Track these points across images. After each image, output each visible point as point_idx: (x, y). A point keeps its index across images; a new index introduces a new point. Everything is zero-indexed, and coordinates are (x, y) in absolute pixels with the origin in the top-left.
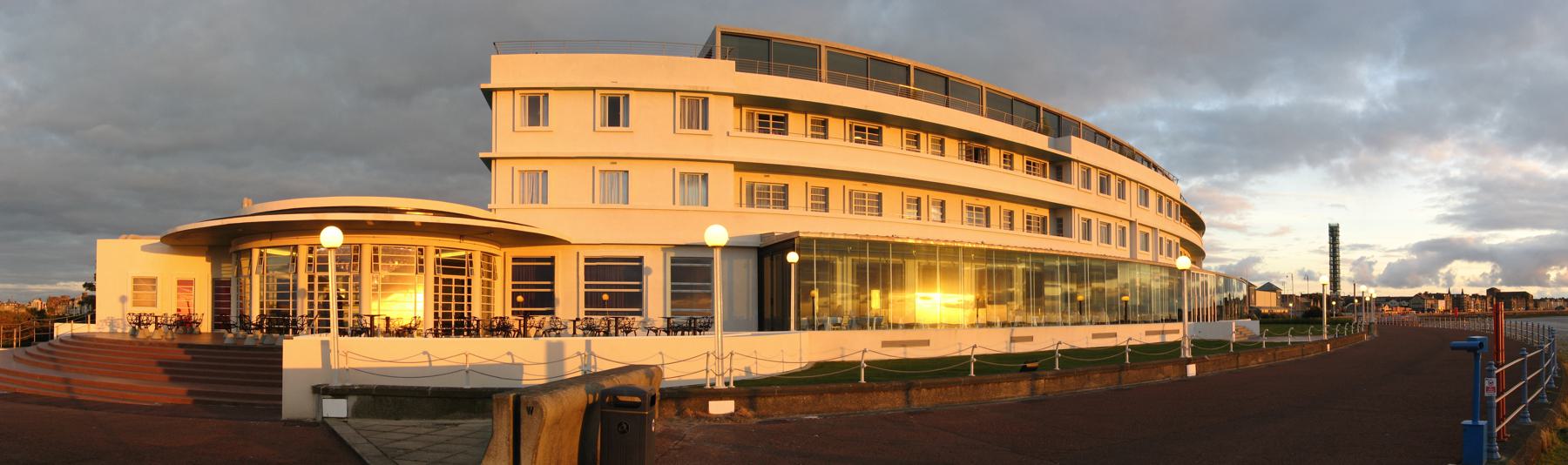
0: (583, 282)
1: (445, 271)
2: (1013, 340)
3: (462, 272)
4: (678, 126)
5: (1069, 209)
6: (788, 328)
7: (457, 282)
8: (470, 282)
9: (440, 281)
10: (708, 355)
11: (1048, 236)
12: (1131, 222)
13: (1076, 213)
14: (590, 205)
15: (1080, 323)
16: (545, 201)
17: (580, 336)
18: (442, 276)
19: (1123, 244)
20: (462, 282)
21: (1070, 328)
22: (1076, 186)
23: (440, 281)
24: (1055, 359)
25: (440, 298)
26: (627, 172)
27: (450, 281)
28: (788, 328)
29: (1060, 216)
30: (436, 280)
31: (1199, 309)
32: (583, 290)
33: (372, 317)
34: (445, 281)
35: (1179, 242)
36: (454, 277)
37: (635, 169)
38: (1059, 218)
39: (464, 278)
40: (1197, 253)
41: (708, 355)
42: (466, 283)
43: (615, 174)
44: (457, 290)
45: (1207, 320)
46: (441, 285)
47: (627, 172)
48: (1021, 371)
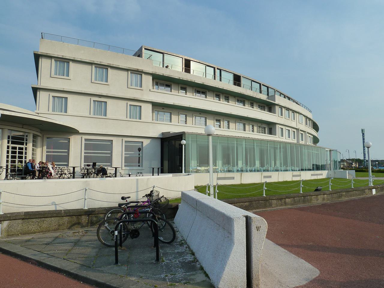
0: (83, 151)
1: (13, 143)
2: (300, 176)
3: (23, 144)
4: (129, 85)
5: (275, 124)
6: (182, 172)
7: (20, 148)
8: (26, 149)
9: (10, 148)
10: (86, 190)
11: (266, 135)
12: (296, 129)
13: (277, 126)
14: (88, 115)
15: (287, 170)
16: (66, 112)
17: (55, 178)
18: (11, 145)
19: (294, 138)
20: (22, 149)
21: (283, 172)
22: (277, 115)
23: (10, 148)
24: (263, 190)
25: (10, 157)
26: (106, 102)
27: (15, 148)
28: (182, 172)
29: (270, 127)
30: (8, 147)
31: (327, 165)
32: (83, 154)
33: (74, 168)
34: (13, 148)
35: (312, 137)
36: (18, 146)
37: (70, 97)
38: (270, 127)
39: (24, 146)
40: (316, 140)
41: (86, 190)
42: (24, 149)
43: (60, 99)
44: (20, 153)
45: (328, 170)
46: (10, 150)
47: (106, 102)
48: (315, 191)
